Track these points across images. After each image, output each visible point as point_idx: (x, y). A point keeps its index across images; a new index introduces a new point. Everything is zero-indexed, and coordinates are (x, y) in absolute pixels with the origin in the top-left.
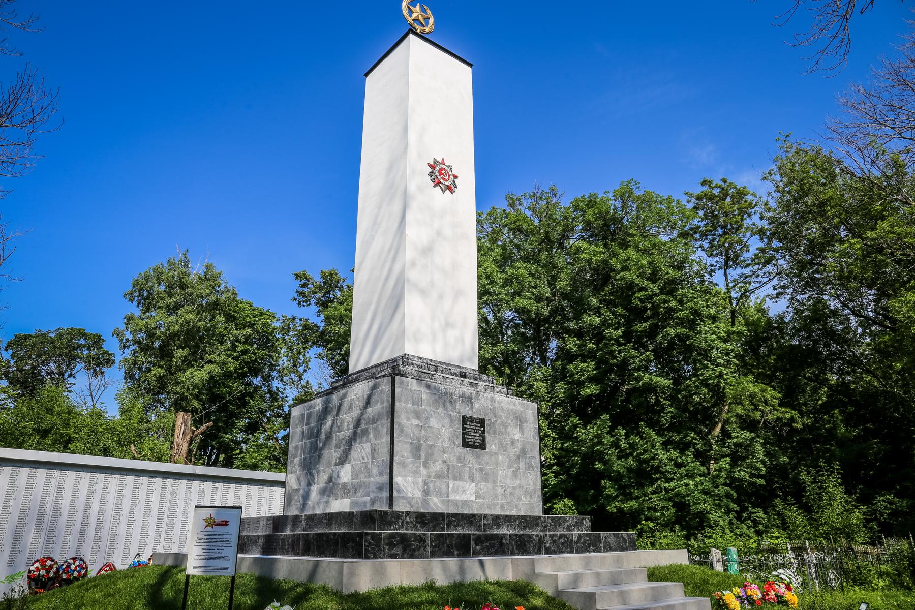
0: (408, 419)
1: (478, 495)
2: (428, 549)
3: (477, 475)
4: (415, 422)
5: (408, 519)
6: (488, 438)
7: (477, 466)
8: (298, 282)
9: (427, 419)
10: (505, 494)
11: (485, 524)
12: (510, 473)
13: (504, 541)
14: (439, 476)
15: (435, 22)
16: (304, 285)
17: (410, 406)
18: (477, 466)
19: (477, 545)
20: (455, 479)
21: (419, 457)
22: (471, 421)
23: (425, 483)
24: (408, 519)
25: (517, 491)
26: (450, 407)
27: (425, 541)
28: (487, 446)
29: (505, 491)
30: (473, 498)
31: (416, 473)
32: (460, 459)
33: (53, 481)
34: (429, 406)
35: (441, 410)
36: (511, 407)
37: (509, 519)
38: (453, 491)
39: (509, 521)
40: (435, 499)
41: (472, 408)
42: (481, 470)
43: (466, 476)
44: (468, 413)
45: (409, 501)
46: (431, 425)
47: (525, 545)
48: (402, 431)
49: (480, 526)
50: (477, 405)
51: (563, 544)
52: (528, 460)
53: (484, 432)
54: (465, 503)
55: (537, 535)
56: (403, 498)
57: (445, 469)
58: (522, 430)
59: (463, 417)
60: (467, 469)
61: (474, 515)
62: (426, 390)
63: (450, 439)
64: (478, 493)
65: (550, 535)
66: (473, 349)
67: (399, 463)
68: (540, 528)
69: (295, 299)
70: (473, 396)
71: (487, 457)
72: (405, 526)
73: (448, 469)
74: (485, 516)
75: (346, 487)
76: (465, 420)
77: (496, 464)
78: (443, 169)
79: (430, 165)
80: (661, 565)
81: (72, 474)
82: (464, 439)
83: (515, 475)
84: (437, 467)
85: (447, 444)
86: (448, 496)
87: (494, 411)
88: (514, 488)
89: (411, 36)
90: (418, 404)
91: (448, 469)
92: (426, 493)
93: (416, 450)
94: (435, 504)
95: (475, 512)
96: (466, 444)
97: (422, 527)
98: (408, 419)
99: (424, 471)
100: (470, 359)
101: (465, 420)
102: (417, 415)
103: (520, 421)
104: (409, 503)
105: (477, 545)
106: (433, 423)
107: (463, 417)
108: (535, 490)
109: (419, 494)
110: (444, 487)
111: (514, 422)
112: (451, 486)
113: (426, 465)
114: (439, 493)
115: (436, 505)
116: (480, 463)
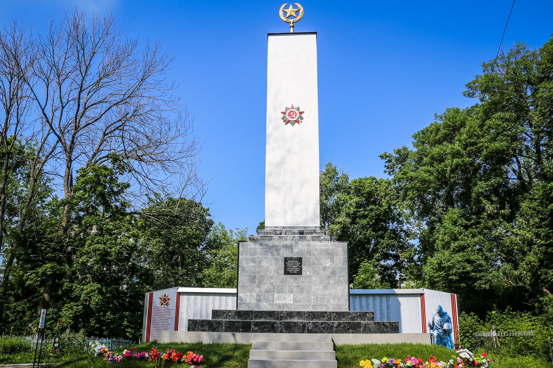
0: (247, 264)
1: (295, 301)
2: (224, 328)
3: (295, 289)
4: (253, 264)
5: (230, 314)
6: (304, 268)
7: (295, 285)
8: (384, 161)
9: (260, 262)
10: (317, 299)
11: (281, 316)
12: (321, 286)
13: (275, 325)
14: (267, 291)
15: (304, 10)
16: (390, 161)
17: (249, 256)
18: (295, 285)
19: (255, 327)
20: (279, 292)
21: (255, 283)
22: (291, 260)
23: (258, 295)
24: (230, 314)
25: (327, 297)
26: (276, 254)
27: (222, 324)
28: (303, 272)
29: (317, 298)
30: (292, 302)
31: (251, 291)
32: (282, 281)
33: (204, 301)
34: (261, 255)
35: (269, 256)
36: (324, 248)
37: (299, 314)
38: (277, 299)
39: (300, 315)
40: (265, 304)
41: (292, 252)
42: (298, 286)
43: (287, 290)
44: (289, 255)
45: (248, 304)
46: (263, 265)
47: (291, 328)
48: (243, 270)
49: (278, 317)
50: (296, 250)
51: (323, 328)
52: (337, 278)
53: (301, 265)
54: (285, 305)
55: (302, 323)
56: (244, 303)
57: (271, 287)
58: (332, 261)
59: (286, 258)
60: (287, 286)
61: (274, 312)
62: (259, 247)
63: (275, 271)
64: (295, 299)
65: (313, 323)
66: (315, 213)
67: (242, 286)
68: (325, 319)
69: (385, 172)
70: (293, 245)
71: (303, 279)
72: (228, 317)
73: (274, 288)
74: (282, 312)
75: (250, 298)
76: (286, 260)
77: (310, 282)
78: (289, 115)
79: (283, 113)
80: (384, 343)
81: (211, 297)
82: (285, 270)
83: (325, 287)
84: (264, 287)
85: (273, 274)
86: (273, 302)
87: (309, 253)
88: (324, 295)
89: (270, 38)
90: (254, 255)
91: (274, 288)
92: (259, 300)
93: (253, 279)
94: (265, 306)
95: (293, 310)
96: (286, 273)
97: (238, 318)
98: (247, 264)
99: (257, 290)
100: (313, 220)
101: (286, 260)
102: (253, 261)
103: (331, 255)
104: (248, 306)
105: (255, 327)
106: (264, 264)
107: (286, 258)
108: (342, 296)
109: (253, 301)
110: (271, 298)
111: (327, 256)
112: (276, 296)
113: (258, 286)
114: (267, 300)
115: (265, 307)
116: (297, 283)
